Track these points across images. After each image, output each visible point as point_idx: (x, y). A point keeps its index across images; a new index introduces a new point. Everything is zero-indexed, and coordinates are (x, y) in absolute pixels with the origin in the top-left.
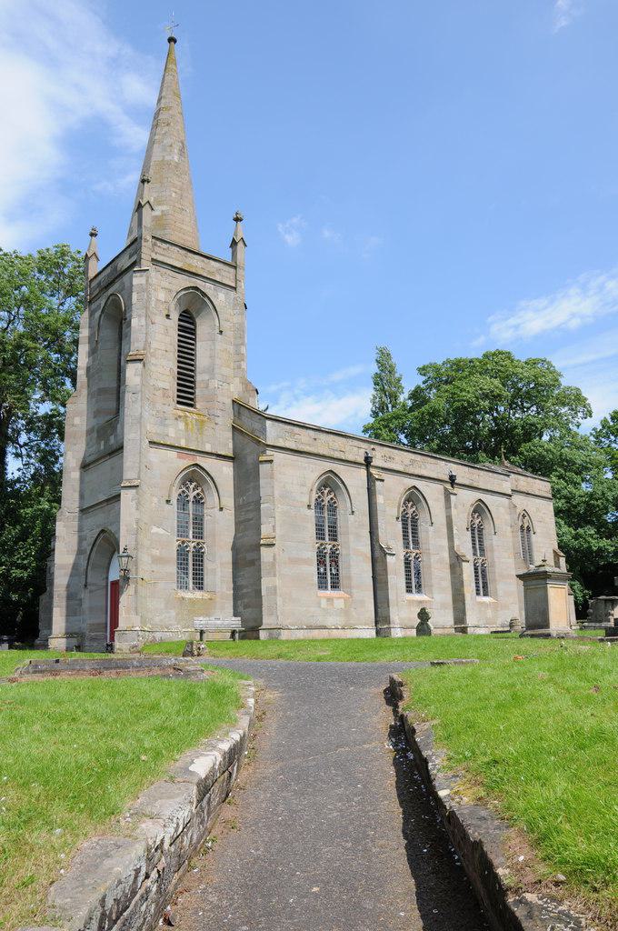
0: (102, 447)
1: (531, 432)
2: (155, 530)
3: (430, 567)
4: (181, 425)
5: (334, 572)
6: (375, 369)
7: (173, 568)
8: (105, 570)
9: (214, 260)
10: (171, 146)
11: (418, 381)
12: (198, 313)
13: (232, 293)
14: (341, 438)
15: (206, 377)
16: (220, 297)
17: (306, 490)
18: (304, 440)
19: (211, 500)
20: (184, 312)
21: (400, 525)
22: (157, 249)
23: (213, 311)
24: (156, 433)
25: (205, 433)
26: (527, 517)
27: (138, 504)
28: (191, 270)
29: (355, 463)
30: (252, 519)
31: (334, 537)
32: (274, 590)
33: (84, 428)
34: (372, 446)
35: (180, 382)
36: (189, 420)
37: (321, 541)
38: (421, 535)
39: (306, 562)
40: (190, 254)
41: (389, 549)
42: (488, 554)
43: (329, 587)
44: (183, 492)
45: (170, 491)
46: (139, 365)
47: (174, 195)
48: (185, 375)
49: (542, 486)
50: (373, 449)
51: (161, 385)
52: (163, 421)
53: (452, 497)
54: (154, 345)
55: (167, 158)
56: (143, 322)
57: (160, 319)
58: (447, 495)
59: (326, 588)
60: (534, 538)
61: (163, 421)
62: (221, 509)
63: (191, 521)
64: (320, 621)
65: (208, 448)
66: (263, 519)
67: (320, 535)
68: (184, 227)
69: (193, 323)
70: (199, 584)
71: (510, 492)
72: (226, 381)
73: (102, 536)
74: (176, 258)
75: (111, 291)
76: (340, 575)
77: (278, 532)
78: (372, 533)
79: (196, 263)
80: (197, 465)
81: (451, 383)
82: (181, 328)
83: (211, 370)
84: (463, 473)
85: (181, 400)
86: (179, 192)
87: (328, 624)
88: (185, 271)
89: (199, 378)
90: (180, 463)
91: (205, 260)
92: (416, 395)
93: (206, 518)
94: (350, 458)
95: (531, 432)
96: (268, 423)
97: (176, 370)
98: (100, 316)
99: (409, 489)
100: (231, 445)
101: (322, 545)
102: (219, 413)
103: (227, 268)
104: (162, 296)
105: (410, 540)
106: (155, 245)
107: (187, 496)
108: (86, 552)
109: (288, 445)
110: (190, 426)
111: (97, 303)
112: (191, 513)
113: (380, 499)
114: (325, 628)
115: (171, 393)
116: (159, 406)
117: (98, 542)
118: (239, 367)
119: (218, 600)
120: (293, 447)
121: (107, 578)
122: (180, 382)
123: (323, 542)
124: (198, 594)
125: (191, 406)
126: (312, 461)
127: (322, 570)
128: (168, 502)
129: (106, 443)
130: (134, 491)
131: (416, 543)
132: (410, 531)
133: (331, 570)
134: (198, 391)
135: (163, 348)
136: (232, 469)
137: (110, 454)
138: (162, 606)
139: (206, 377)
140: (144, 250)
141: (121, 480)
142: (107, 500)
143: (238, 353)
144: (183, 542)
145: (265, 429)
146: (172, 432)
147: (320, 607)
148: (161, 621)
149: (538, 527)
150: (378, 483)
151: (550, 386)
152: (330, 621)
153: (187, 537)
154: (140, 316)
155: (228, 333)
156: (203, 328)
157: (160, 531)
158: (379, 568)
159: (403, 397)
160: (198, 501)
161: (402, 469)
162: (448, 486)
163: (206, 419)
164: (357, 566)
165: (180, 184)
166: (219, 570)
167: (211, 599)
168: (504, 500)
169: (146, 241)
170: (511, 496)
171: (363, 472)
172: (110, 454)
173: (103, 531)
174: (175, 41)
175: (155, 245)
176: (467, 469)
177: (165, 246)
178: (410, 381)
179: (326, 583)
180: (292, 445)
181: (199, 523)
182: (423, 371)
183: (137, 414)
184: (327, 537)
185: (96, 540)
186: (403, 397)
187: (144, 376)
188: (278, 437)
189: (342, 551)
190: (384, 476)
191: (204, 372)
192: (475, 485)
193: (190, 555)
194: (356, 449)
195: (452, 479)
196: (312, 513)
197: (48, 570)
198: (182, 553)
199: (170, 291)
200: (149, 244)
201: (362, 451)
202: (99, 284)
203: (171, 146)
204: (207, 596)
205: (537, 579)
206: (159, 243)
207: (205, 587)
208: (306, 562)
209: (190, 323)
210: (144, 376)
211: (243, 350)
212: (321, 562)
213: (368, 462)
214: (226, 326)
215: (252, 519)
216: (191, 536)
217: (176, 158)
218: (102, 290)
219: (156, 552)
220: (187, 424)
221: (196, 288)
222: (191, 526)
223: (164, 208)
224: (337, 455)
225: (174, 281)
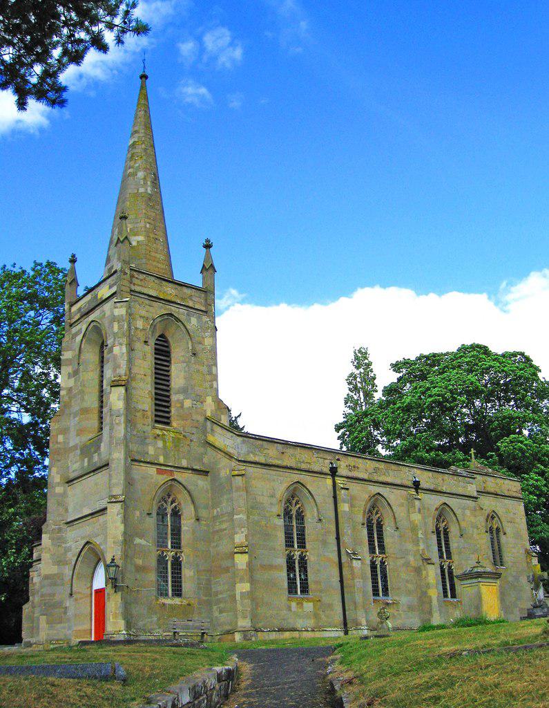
0: (86, 464)
1: (508, 427)
5: (303, 577)
7: (152, 576)
8: (89, 580)
9: (261, 464)
11: (393, 377)
13: (205, 319)
15: (181, 397)
18: (272, 454)
20: (159, 336)
28: (166, 298)
29: (321, 473)
30: (225, 529)
31: (302, 544)
35: (157, 402)
36: (167, 438)
37: (442, 560)
38: (387, 540)
41: (354, 554)
42: (455, 557)
47: (148, 226)
49: (512, 485)
50: (338, 460)
59: (296, 593)
60: (503, 539)
63: (169, 532)
64: (291, 622)
65: (184, 463)
67: (289, 543)
68: (158, 256)
70: (178, 592)
71: (475, 494)
73: (87, 547)
74: (152, 288)
75: (92, 317)
76: (309, 580)
79: (169, 291)
81: (425, 378)
84: (426, 478)
86: (152, 222)
87: (299, 626)
89: (174, 398)
91: (177, 286)
92: (390, 391)
94: (316, 468)
95: (508, 427)
97: (153, 391)
98: (82, 340)
99: (374, 496)
103: (198, 294)
105: (376, 544)
107: (166, 509)
108: (71, 563)
109: (256, 459)
111: (78, 327)
112: (169, 524)
114: (295, 630)
115: (149, 413)
117: (83, 553)
121: (92, 586)
122: (157, 402)
123: (292, 549)
124: (177, 601)
126: (281, 472)
127: (303, 577)
129: (89, 461)
132: (375, 536)
133: (300, 576)
134: (173, 410)
135: (142, 373)
137: (94, 471)
138: (145, 612)
142: (92, 514)
147: (290, 610)
148: (144, 625)
149: (508, 528)
151: (527, 379)
152: (300, 624)
153: (293, 546)
157: (143, 542)
159: (378, 396)
161: (366, 477)
162: (413, 492)
163: (182, 437)
168: (470, 503)
170: (476, 498)
171: (329, 481)
172: (94, 471)
173: (88, 543)
174: (146, 77)
175: (132, 276)
176: (430, 474)
177: (142, 277)
178: (385, 377)
179: (296, 588)
180: (262, 460)
182: (396, 367)
185: (81, 552)
186: (378, 396)
188: (249, 453)
191: (178, 392)
194: (321, 460)
195: (416, 485)
197: (30, 582)
198: (161, 560)
201: (328, 461)
202: (80, 309)
204: (185, 602)
205: (471, 578)
207: (183, 595)
209: (164, 341)
212: (291, 568)
213: (334, 472)
215: (225, 529)
216: (169, 546)
218: (82, 317)
220: (165, 442)
221: (171, 315)
222: (169, 536)
224: (303, 466)
225: (151, 309)
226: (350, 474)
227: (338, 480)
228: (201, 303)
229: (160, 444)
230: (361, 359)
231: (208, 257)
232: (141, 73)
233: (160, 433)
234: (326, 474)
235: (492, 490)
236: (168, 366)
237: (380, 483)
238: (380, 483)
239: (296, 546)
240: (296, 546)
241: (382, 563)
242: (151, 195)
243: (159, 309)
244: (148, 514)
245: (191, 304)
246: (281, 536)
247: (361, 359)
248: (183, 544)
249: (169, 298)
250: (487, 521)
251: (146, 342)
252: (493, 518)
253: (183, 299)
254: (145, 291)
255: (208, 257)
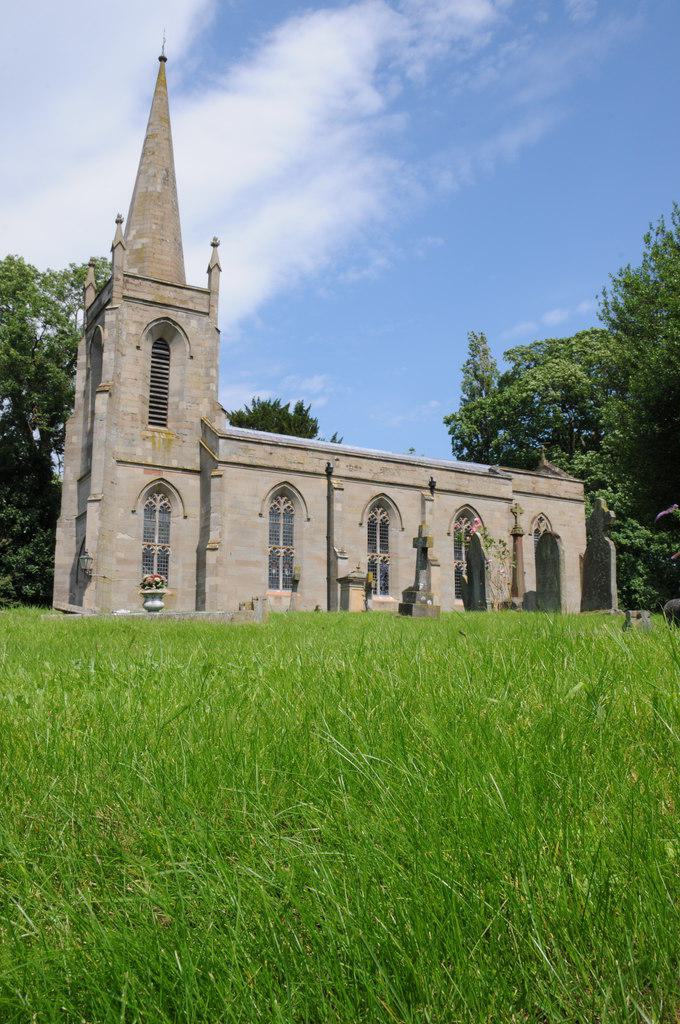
2: (120, 536)
3: (397, 570)
4: (149, 445)
6: (465, 356)
9: (245, 465)
10: (155, 176)
12: (171, 341)
13: (206, 319)
14: (300, 451)
15: (177, 399)
16: (191, 325)
17: (258, 500)
19: (177, 509)
21: (365, 531)
22: (129, 286)
23: (185, 339)
24: (124, 453)
25: (172, 450)
26: (545, 521)
27: (102, 514)
32: (215, 588)
33: (80, 446)
34: (336, 457)
36: (156, 440)
38: (391, 539)
39: (256, 564)
40: (162, 286)
41: (342, 553)
43: (281, 586)
44: (275, 506)
45: (136, 502)
46: (106, 395)
47: (154, 227)
48: (157, 397)
50: (337, 460)
51: (130, 410)
52: (131, 442)
53: (428, 503)
54: (124, 375)
55: (151, 189)
56: (113, 355)
57: (130, 351)
58: (424, 500)
59: (278, 587)
61: (131, 442)
62: (185, 517)
63: (157, 527)
65: (175, 464)
66: (212, 526)
68: (163, 257)
69: (168, 350)
72: (195, 401)
74: (147, 292)
77: (226, 536)
78: (329, 538)
79: (168, 294)
80: (162, 479)
82: (155, 355)
83: (180, 394)
85: (163, 417)
88: (156, 303)
89: (171, 400)
90: (145, 478)
91: (178, 290)
93: (172, 525)
96: (221, 441)
99: (377, 496)
100: (198, 460)
101: (275, 549)
102: (186, 432)
104: (133, 329)
106: (127, 282)
110: (157, 445)
113: (337, 507)
116: (128, 430)
118: (208, 388)
119: (179, 596)
120: (247, 461)
125: (165, 425)
127: (274, 571)
128: (261, 515)
130: (97, 504)
131: (385, 547)
134: (169, 412)
136: (199, 482)
139: (177, 399)
140: (115, 288)
141: (89, 494)
143: (207, 375)
144: (149, 546)
145: (218, 445)
146: (139, 451)
150: (336, 492)
153: (278, 544)
154: (110, 350)
155: (200, 357)
156: (177, 354)
157: (126, 536)
158: (332, 570)
160: (165, 510)
161: (369, 477)
162: (427, 493)
164: (313, 573)
165: (162, 214)
166: (181, 570)
167: (172, 595)
169: (118, 280)
171: (324, 482)
177: (136, 281)
179: (278, 583)
181: (165, 527)
183: (104, 439)
184: (281, 543)
187: (112, 408)
189: (296, 554)
190: (346, 484)
192: (463, 490)
193: (156, 557)
195: (432, 486)
196: (266, 520)
199: (141, 323)
200: (121, 283)
203: (155, 176)
206: (130, 280)
208: (256, 564)
210: (112, 408)
211: (213, 372)
213: (329, 473)
214: (197, 351)
217: (159, 189)
219: (121, 555)
220: (154, 443)
222: (157, 532)
223: (144, 240)
224: (294, 467)
226: (351, 475)
227: (334, 481)
228: (203, 305)
229: (149, 445)
230: (477, 346)
231: (214, 256)
232: (160, 54)
233: (149, 434)
234: (320, 474)
235: (544, 492)
236: (167, 369)
237: (387, 483)
238: (387, 483)
239: (156, 540)
240: (156, 540)
241: (384, 561)
242: (160, 194)
243: (156, 313)
244: (133, 512)
245: (191, 306)
246: (264, 534)
247: (477, 346)
248: (171, 539)
249: (166, 302)
250: (532, 523)
251: (138, 348)
252: (541, 520)
253: (185, 302)
254: (141, 296)
255: (214, 256)
